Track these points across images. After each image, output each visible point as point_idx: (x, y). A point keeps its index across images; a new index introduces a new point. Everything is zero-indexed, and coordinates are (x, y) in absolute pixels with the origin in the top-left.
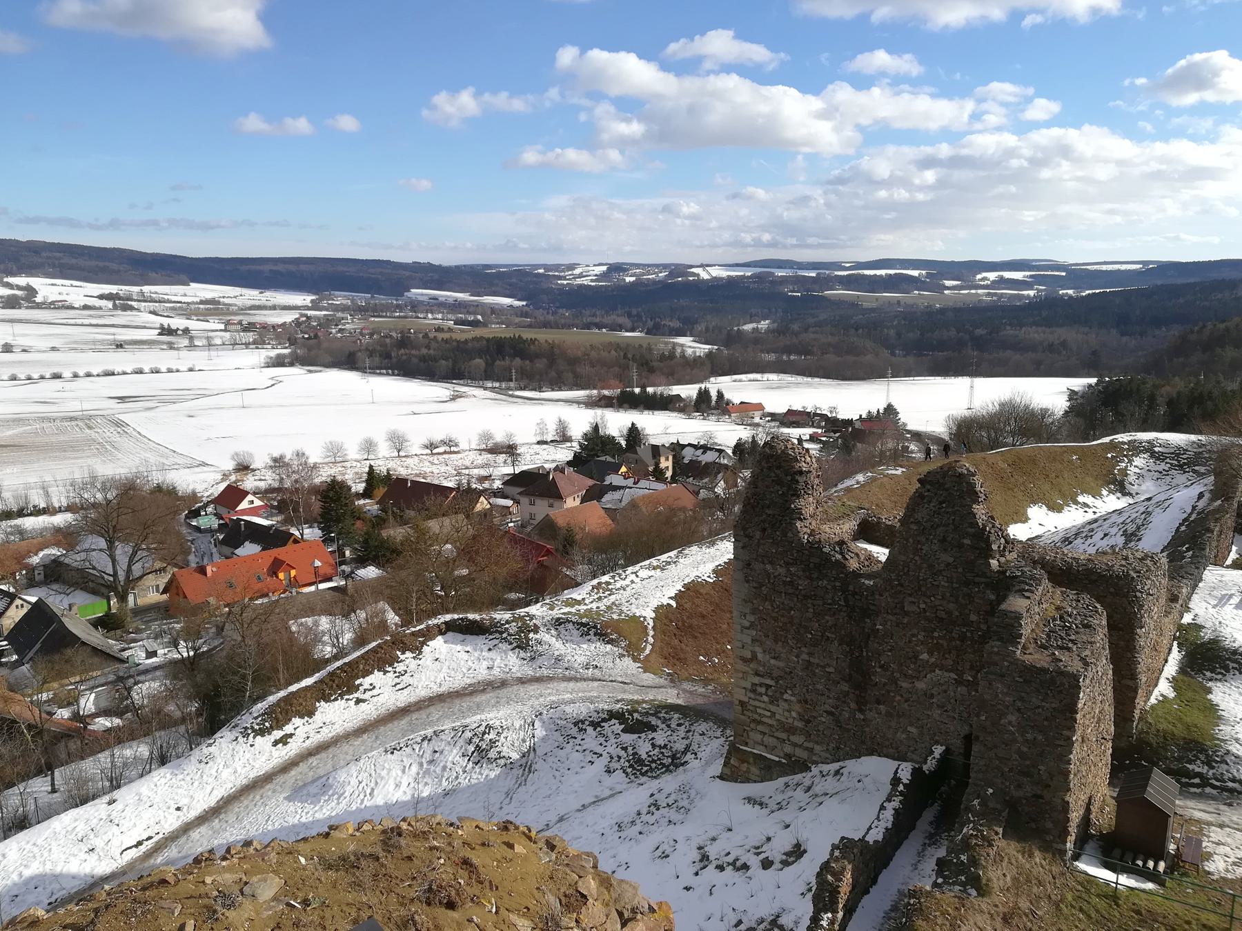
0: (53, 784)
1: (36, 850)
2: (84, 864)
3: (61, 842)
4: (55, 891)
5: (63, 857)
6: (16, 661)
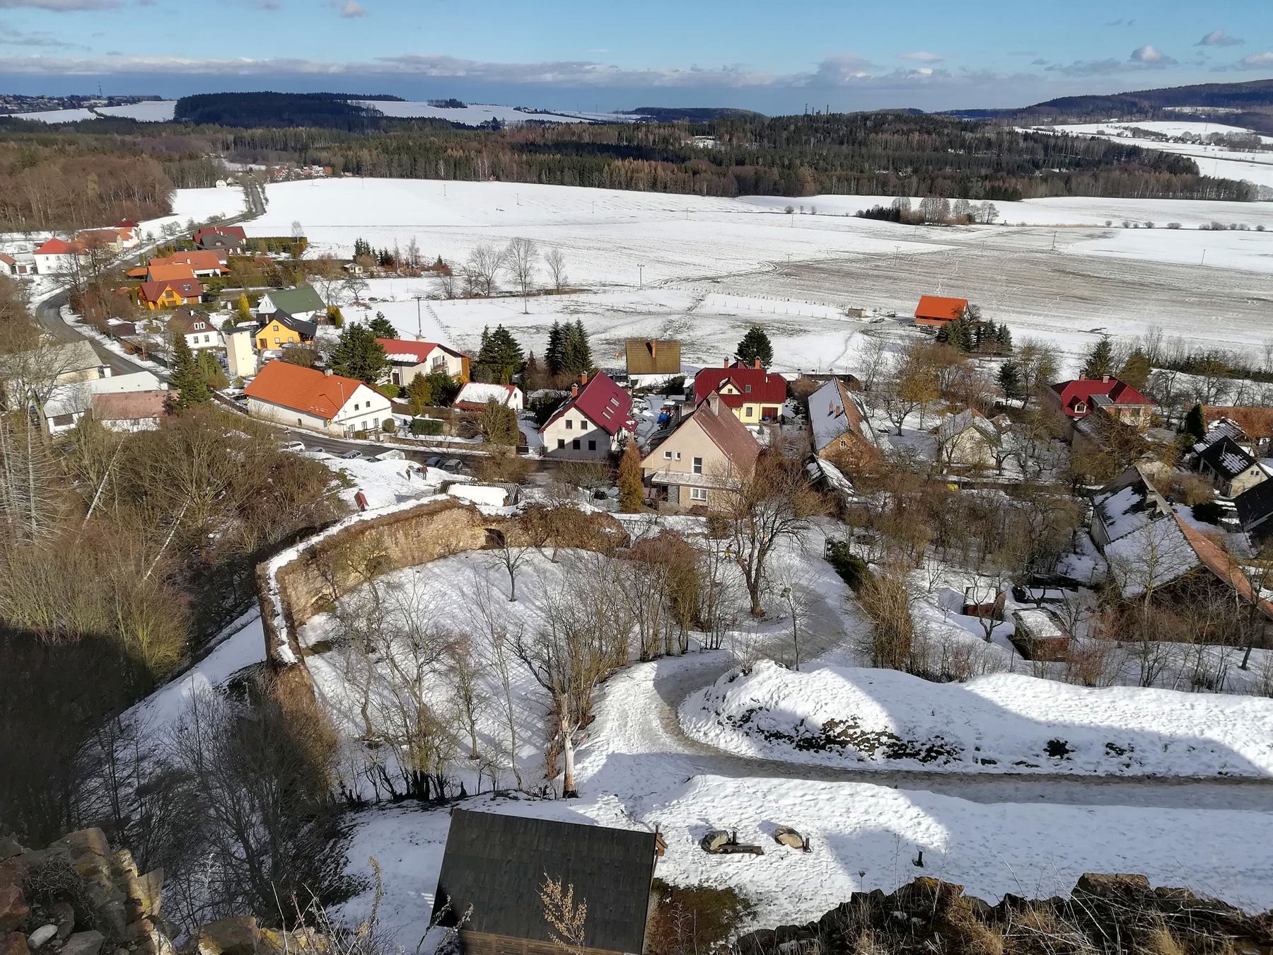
0: (1245, 662)
1: (1221, 717)
2: (1262, 756)
3: (1247, 723)
4: (1228, 765)
5: (1245, 738)
6: (1236, 525)
